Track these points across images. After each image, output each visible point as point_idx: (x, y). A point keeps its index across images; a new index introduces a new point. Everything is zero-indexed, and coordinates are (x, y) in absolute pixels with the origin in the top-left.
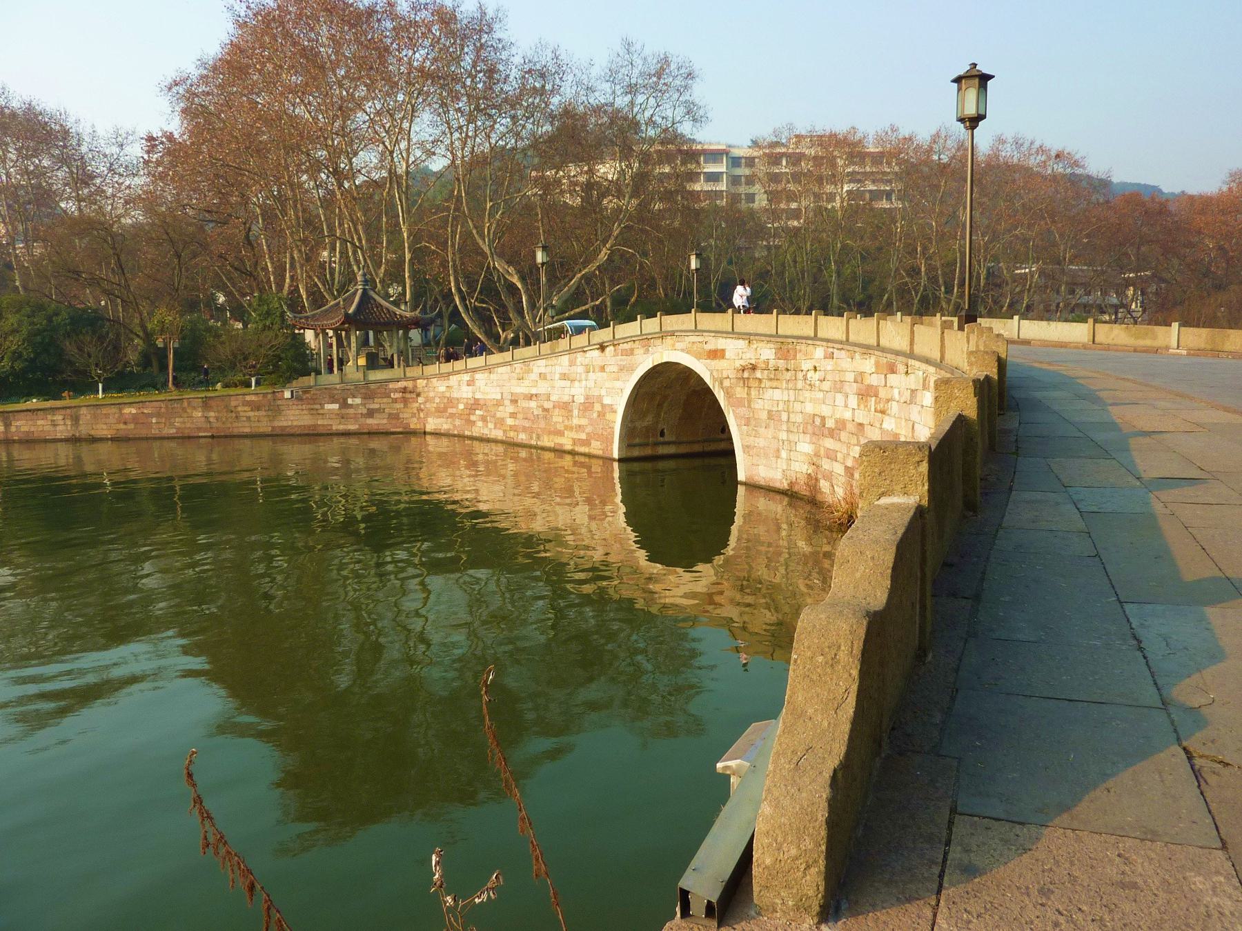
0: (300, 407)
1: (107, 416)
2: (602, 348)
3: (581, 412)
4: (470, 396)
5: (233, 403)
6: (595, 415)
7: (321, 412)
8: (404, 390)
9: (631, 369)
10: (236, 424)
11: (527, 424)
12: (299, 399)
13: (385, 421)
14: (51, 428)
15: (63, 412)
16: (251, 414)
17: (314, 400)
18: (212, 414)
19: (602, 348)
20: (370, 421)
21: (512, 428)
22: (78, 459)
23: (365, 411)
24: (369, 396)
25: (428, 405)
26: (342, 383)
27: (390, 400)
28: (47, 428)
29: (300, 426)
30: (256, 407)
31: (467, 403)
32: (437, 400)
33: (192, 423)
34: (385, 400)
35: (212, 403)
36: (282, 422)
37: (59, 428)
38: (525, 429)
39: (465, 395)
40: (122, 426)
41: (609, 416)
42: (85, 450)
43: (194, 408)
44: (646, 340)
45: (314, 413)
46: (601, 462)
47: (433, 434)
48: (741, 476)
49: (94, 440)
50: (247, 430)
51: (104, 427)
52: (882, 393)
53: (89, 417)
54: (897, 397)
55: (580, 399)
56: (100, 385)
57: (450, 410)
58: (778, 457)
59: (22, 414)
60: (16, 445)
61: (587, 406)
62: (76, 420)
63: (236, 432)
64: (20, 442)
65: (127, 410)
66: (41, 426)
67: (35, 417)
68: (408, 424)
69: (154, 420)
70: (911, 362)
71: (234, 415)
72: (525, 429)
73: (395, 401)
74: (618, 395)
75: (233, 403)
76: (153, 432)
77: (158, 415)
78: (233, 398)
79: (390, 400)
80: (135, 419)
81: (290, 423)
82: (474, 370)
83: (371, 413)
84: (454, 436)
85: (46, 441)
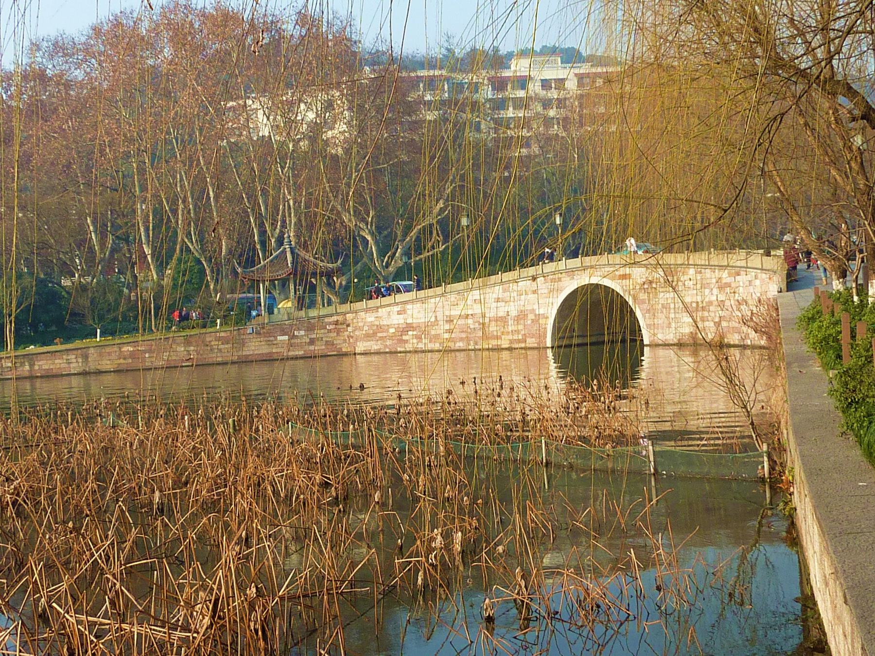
0: (259, 340)
1: (109, 354)
2: (534, 279)
3: (516, 322)
4: (402, 321)
5: (208, 339)
6: (529, 322)
7: (275, 342)
8: (336, 323)
9: (559, 290)
10: (211, 355)
11: (464, 335)
12: (258, 333)
13: (323, 347)
14: (67, 365)
15: (75, 352)
16: (221, 347)
17: (269, 334)
18: (192, 348)
19: (534, 279)
20: (312, 348)
21: (448, 340)
22: (87, 389)
23: (308, 340)
24: (310, 328)
25: (357, 333)
26: (289, 319)
27: (326, 331)
28: (63, 366)
29: (260, 354)
30: (225, 341)
31: (399, 327)
32: (366, 328)
33: (177, 356)
34: (322, 331)
35: (193, 340)
36: (247, 352)
37: (72, 365)
38: (461, 339)
39: (396, 322)
40: (122, 361)
41: (542, 321)
42: (93, 380)
43: (178, 344)
44: (571, 272)
45: (270, 344)
46: (536, 352)
47: (363, 354)
48: (646, 342)
49: (100, 372)
50: (220, 359)
51: (108, 362)
52: (733, 285)
53: (95, 356)
54: (742, 285)
55: (514, 313)
56: (98, 331)
57: (379, 335)
58: (670, 327)
59: (43, 355)
60: (39, 380)
61: (521, 316)
62: (86, 357)
63: (211, 361)
64: (42, 377)
65: (125, 349)
66: (58, 364)
67: (54, 358)
68: (341, 349)
69: (147, 355)
70: (748, 270)
71: (209, 348)
72: (461, 339)
73: (330, 331)
74: (550, 309)
75: (208, 339)
76: (147, 364)
77: (150, 351)
78: (207, 335)
79: (326, 331)
80: (132, 355)
81: (251, 353)
82: (405, 302)
83: (312, 342)
84: (387, 353)
85: (63, 375)
